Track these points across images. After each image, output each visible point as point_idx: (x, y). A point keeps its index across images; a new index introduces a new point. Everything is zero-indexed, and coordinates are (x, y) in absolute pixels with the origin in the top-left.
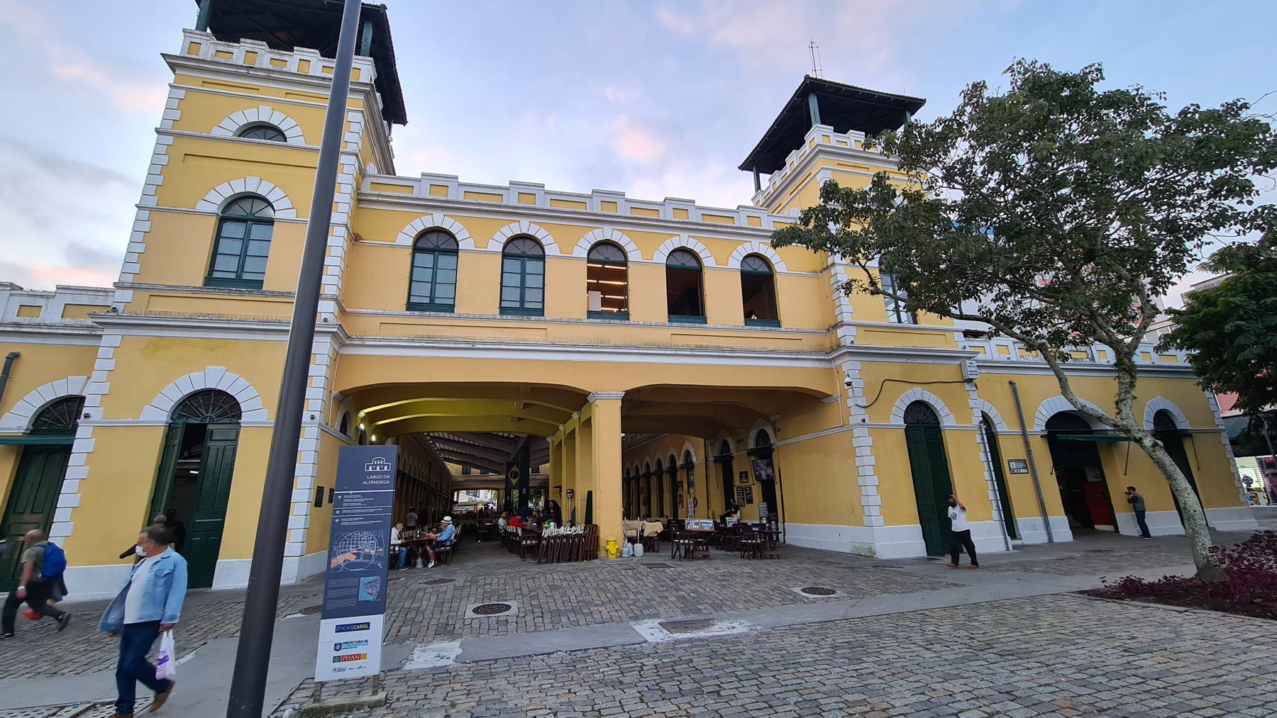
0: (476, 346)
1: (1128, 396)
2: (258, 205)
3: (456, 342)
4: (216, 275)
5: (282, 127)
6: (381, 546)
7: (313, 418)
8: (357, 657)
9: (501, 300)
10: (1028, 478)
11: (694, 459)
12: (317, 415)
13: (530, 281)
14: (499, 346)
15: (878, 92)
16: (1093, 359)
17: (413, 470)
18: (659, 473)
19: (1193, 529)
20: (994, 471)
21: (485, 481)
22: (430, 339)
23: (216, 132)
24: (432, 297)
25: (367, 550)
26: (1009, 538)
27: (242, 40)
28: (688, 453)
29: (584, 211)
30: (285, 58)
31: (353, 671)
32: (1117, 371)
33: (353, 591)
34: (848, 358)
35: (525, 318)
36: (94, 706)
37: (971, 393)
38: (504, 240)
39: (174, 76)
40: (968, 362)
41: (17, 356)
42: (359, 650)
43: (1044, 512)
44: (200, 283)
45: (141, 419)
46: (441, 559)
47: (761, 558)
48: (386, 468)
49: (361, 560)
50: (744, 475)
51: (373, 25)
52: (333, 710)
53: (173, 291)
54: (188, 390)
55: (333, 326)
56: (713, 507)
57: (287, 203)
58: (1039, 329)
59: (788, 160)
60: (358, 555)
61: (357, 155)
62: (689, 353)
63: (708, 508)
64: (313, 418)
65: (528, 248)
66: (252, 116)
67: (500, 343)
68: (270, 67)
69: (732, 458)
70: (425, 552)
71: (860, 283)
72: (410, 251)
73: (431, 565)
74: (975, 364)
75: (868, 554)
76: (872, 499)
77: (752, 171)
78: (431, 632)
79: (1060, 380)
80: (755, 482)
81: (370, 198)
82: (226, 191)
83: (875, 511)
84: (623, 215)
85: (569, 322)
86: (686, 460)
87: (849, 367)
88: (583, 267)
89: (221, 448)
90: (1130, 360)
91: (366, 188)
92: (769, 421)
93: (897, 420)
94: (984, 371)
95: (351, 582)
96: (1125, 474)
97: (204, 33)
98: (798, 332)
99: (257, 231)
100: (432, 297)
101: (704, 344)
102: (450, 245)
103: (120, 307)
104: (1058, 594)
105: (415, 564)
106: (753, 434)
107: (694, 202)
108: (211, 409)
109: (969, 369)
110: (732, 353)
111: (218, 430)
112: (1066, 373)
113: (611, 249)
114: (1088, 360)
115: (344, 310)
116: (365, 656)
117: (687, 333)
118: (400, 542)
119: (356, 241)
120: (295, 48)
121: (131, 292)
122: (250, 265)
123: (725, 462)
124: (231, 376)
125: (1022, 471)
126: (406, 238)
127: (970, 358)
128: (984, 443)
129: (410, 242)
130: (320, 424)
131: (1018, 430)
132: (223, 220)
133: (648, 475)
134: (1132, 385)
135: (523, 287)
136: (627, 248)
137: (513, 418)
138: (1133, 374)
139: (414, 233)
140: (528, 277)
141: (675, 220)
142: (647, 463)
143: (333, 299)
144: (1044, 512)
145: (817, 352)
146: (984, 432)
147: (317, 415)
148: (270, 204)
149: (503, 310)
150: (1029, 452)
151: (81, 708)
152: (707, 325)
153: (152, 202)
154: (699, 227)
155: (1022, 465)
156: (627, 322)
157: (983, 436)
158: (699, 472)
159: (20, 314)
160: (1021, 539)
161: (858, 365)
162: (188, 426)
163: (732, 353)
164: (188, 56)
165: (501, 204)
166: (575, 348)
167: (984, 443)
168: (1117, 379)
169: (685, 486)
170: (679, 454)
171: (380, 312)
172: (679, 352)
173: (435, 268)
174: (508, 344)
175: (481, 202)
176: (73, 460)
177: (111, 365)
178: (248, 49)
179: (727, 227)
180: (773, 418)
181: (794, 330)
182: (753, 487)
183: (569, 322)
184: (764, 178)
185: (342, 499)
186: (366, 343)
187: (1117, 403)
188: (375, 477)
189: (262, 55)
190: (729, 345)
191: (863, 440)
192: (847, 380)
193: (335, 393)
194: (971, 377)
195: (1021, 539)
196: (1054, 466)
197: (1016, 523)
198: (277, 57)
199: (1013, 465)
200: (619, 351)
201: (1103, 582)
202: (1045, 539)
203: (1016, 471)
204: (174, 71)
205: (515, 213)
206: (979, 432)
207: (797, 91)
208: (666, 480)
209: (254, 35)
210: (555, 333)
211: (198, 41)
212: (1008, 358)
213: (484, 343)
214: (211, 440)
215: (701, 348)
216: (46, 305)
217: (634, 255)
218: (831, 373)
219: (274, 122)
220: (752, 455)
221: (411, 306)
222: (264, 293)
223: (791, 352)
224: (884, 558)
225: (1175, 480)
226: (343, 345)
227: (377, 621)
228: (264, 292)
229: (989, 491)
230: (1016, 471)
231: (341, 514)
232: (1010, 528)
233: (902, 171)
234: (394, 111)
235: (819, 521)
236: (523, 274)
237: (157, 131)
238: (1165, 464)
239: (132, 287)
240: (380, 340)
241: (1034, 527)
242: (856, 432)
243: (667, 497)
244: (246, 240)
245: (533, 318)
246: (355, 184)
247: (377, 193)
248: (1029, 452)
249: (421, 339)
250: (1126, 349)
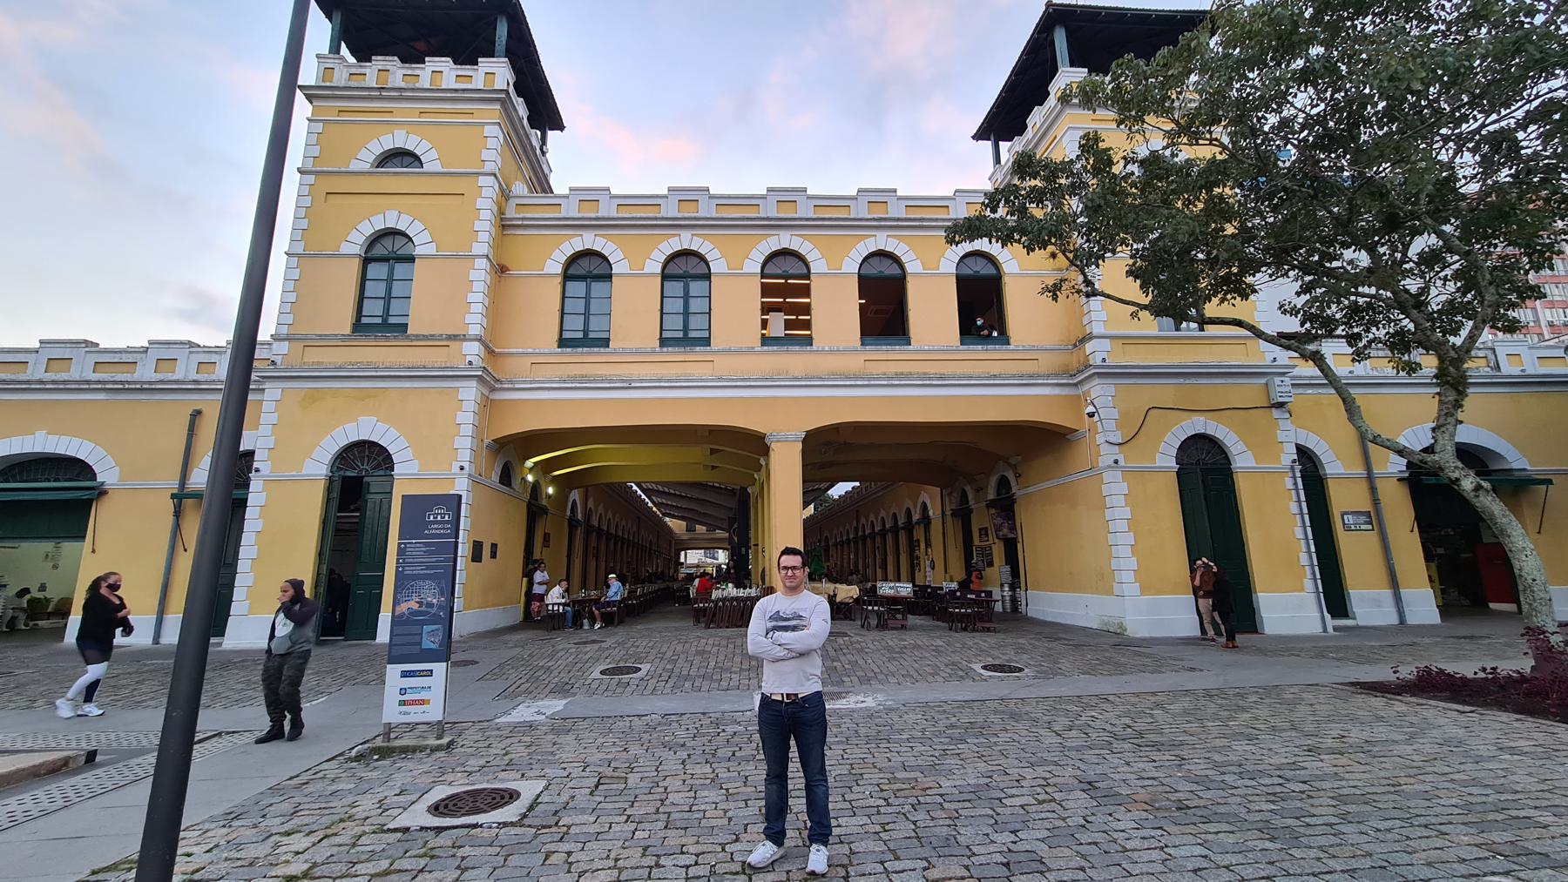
0: (633, 385)
1: (1449, 420)
2: (400, 241)
3: (611, 381)
4: (364, 320)
5: (418, 152)
6: (442, 595)
7: (462, 468)
8: (422, 702)
9: (661, 330)
10: (1373, 538)
11: (931, 513)
12: (466, 465)
13: (695, 306)
14: (659, 383)
15: (1156, 11)
16: (1498, 367)
17: (620, 528)
18: (909, 527)
19: (1531, 605)
20: (1311, 526)
21: (712, 539)
22: (583, 378)
23: (355, 166)
24: (586, 332)
25: (429, 599)
26: (1327, 616)
27: (373, 58)
28: (924, 506)
29: (757, 215)
30: (417, 72)
31: (416, 715)
32: (1437, 385)
33: (417, 639)
34: (1097, 381)
35: (688, 349)
36: (219, 734)
37: (1281, 422)
38: (663, 258)
39: (311, 107)
40: (1277, 380)
41: (199, 412)
42: (423, 696)
43: (1394, 584)
44: (348, 330)
45: (304, 472)
46: (609, 620)
47: (974, 630)
48: (447, 518)
49: (424, 608)
50: (984, 532)
51: (507, 18)
52: (398, 750)
53: (323, 341)
54: (344, 442)
55: (476, 369)
56: (952, 571)
57: (426, 236)
58: (1374, 329)
59: (1030, 121)
60: (420, 603)
61: (495, 175)
62: (885, 383)
63: (946, 572)
64: (462, 468)
65: (692, 266)
66: (389, 143)
67: (659, 380)
68: (403, 85)
69: (971, 511)
70: (591, 612)
71: (1073, 283)
72: (560, 279)
73: (597, 626)
74: (1288, 381)
75: (1119, 631)
76: (1125, 562)
77: (989, 139)
78: (547, 690)
79: (1344, 400)
80: (996, 541)
81: (514, 223)
82: (367, 229)
83: (1128, 577)
84: (805, 216)
85: (739, 352)
86: (923, 515)
87: (1100, 393)
88: (756, 284)
89: (378, 502)
90: (1458, 369)
91: (511, 212)
92: (1009, 464)
93: (1167, 460)
94: (1310, 391)
95: (415, 629)
96: (1539, 533)
97: (337, 56)
98: (1032, 350)
99: (399, 270)
100: (586, 332)
101: (906, 370)
102: (702, 270)
103: (278, 360)
104: (1317, 685)
105: (582, 625)
106: (993, 481)
107: (895, 191)
108: (366, 459)
109: (1278, 389)
110: (942, 380)
111: (375, 483)
112: (1352, 391)
113: (791, 260)
114: (1489, 369)
115: (493, 351)
116: (428, 702)
117: (886, 357)
118: (563, 601)
119: (502, 272)
120: (427, 59)
121: (287, 343)
122: (395, 307)
123: (963, 515)
124: (382, 427)
125: (1363, 527)
126: (555, 266)
127: (1283, 374)
128: (1297, 489)
129: (559, 269)
130: (470, 475)
131: (1362, 471)
132: (367, 261)
133: (883, 532)
134: (1458, 405)
135: (686, 313)
136: (809, 258)
137: (706, 467)
138: (1460, 388)
139: (563, 259)
140: (692, 301)
141: (869, 217)
142: (883, 518)
143: (476, 340)
144: (1394, 584)
145: (1056, 375)
146: (1298, 474)
147: (466, 465)
148: (410, 239)
149: (664, 342)
150: (1376, 501)
151: (209, 734)
152: (910, 347)
153: (299, 249)
154: (900, 223)
155: (1363, 519)
156: (809, 348)
157: (1295, 480)
158: (936, 527)
159: (49, 368)
160: (1355, 618)
161: (1112, 390)
162: (345, 479)
163: (942, 380)
164: (323, 84)
165: (658, 215)
166: (744, 383)
167: (1297, 489)
168: (1437, 397)
169: (923, 546)
170: (915, 507)
171: (530, 350)
172: (872, 382)
173: (588, 298)
174: (668, 381)
175: (634, 215)
176: (249, 512)
177: (274, 418)
178: (380, 67)
179: (936, 220)
180: (1013, 461)
181: (1027, 347)
182: (994, 547)
183: (739, 352)
184: (1004, 146)
185: (405, 547)
186: (517, 386)
187: (1434, 430)
188: (436, 526)
189: (394, 73)
190: (937, 371)
191: (1115, 487)
192: (1090, 409)
193: (487, 441)
194: (1281, 400)
195: (1355, 618)
196: (1416, 518)
197: (1349, 597)
198: (409, 72)
199: (1349, 519)
200: (798, 383)
201: (1395, 672)
202: (1394, 620)
203: (1353, 527)
204: (311, 103)
205: (675, 225)
206: (1290, 475)
207: (1037, 25)
208: (902, 535)
209: (385, 51)
210: (724, 365)
211: (331, 66)
212: (1522, 371)
213: (642, 381)
214: (369, 493)
215: (899, 376)
216: (220, 360)
217: (818, 265)
218: (1078, 402)
219: (409, 147)
220: (993, 507)
221: (563, 343)
222: (408, 338)
223: (1021, 376)
224: (1137, 636)
225: (1509, 536)
226: (493, 389)
227: (439, 668)
228: (409, 336)
229: (1301, 554)
230: (1353, 527)
231: (404, 563)
232: (1335, 599)
233: (1122, 127)
234: (545, 114)
235: (1064, 589)
236: (686, 298)
237: (299, 171)
238: (1493, 514)
239: (288, 338)
240: (531, 382)
241: (1378, 603)
242: (1107, 476)
243: (903, 558)
244: (390, 281)
245: (698, 349)
246: (495, 209)
247: (521, 216)
248: (1376, 501)
249: (573, 379)
250: (1453, 354)
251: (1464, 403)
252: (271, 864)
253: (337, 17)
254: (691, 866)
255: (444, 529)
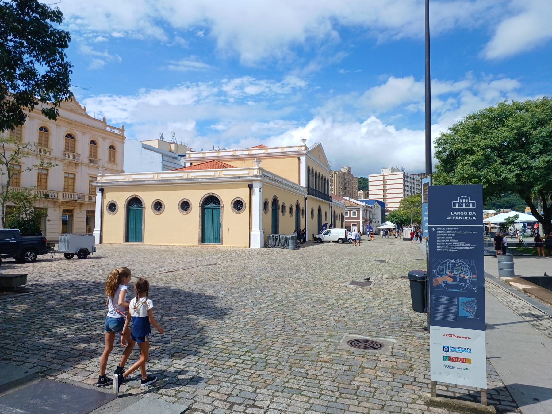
6: (474, 273)
33: (454, 309)
49: (457, 283)
60: (454, 279)
251: (51, 119)
252: (308, 383)
253: (411, 75)
254: (370, 397)
255: (468, 215)
